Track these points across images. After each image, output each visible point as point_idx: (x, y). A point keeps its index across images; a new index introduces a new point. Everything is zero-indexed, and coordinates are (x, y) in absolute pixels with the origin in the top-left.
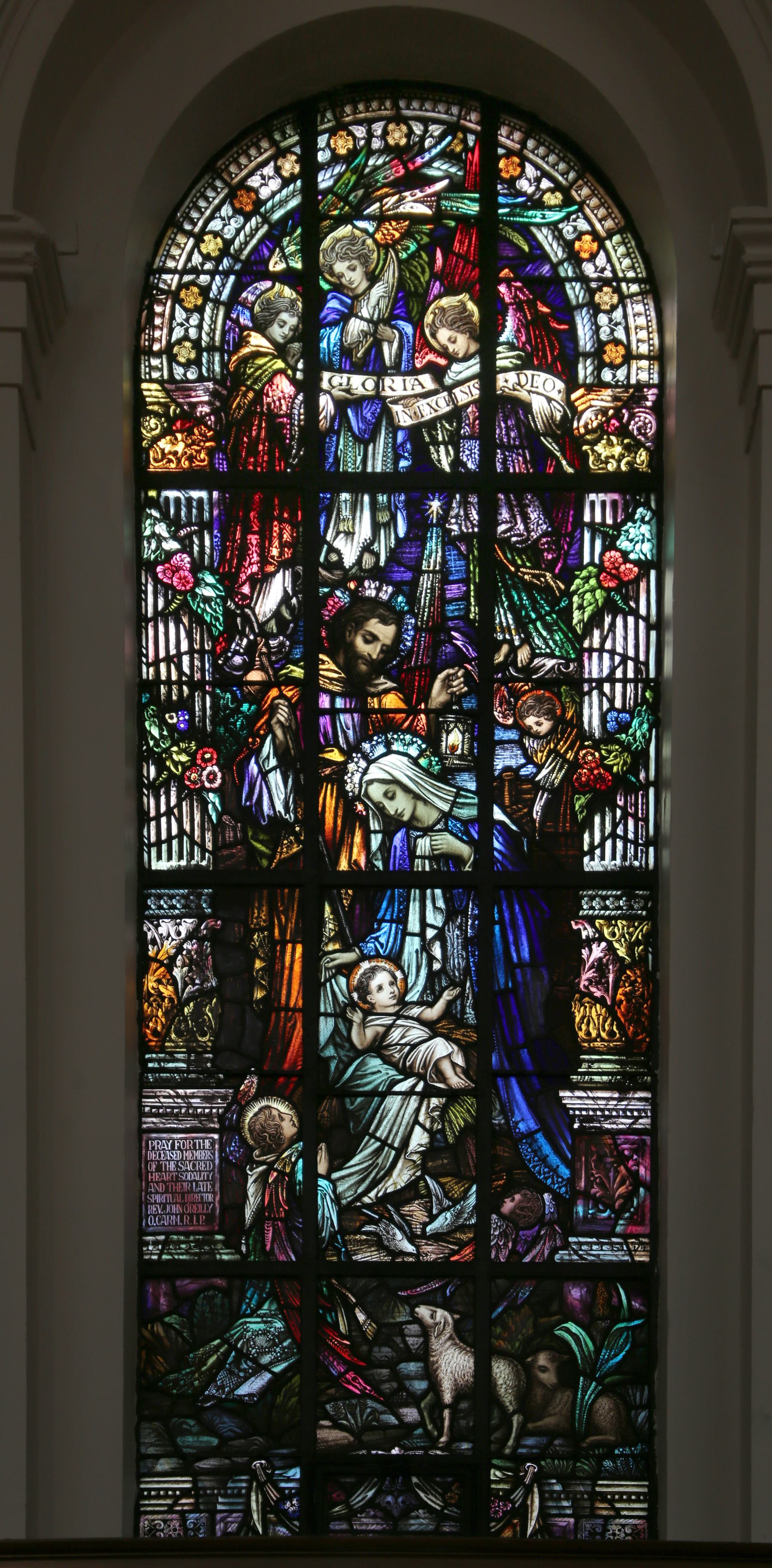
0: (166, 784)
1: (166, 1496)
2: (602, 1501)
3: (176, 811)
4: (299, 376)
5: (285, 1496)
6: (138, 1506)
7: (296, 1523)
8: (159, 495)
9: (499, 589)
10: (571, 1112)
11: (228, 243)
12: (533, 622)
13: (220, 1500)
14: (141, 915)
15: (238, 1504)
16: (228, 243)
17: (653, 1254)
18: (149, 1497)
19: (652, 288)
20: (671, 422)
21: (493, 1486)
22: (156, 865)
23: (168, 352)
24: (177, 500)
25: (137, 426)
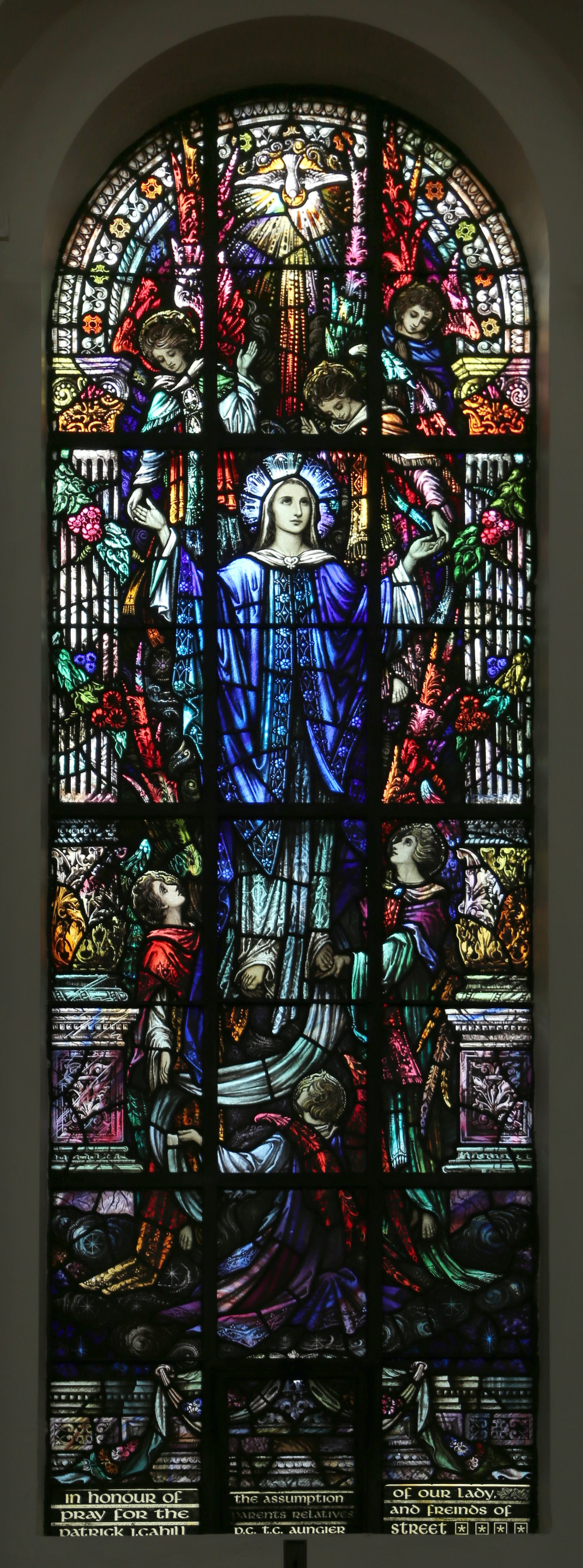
0: (75, 721)
1: (75, 1401)
2: (490, 1397)
3: (85, 747)
4: (201, 390)
5: (188, 1397)
6: (49, 1465)
7: (198, 1424)
8: (71, 455)
9: (382, 643)
10: (457, 1028)
11: (135, 227)
12: (396, 1112)
13: (126, 1404)
14: (52, 843)
15: (111, 667)
16: (135, 227)
17: (534, 1163)
18: (60, 1401)
19: (523, 266)
20: (544, 337)
21: (384, 1384)
22: (65, 798)
23: (79, 325)
24: (89, 462)
25: (51, 394)
